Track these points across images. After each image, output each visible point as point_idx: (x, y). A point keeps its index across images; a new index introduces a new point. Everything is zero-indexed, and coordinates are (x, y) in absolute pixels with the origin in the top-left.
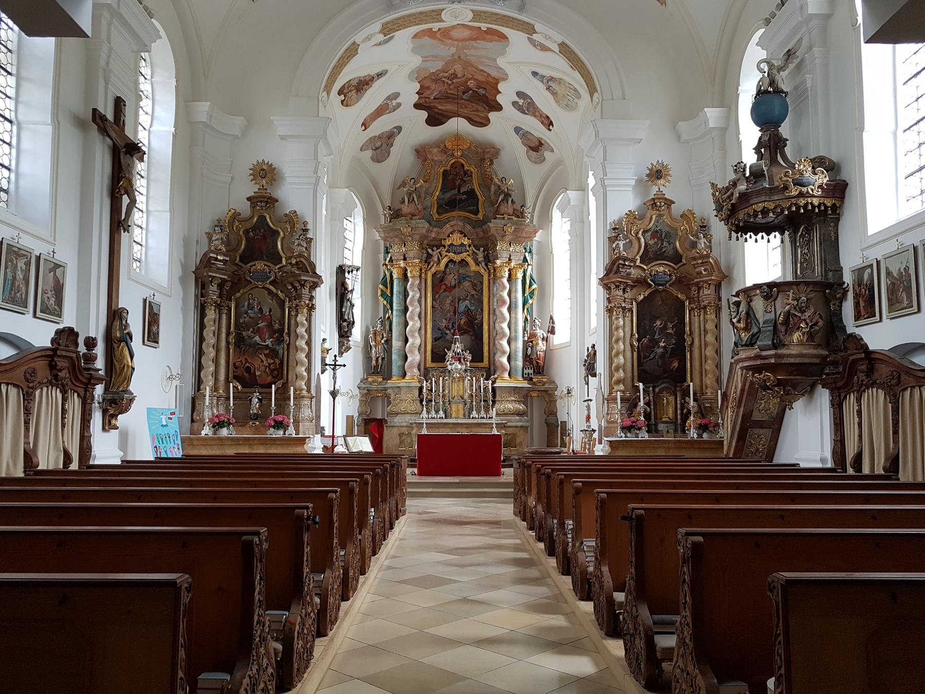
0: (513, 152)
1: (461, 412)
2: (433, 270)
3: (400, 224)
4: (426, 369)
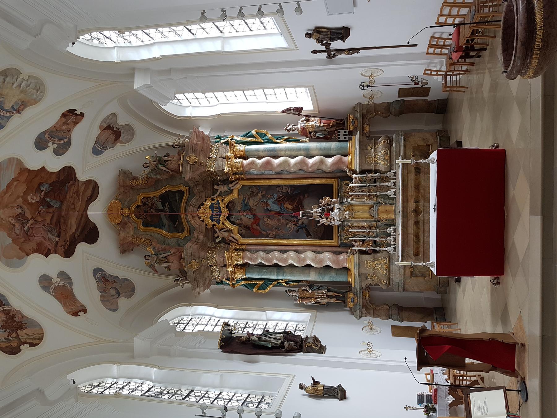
0: (119, 157)
1: (388, 208)
2: (237, 237)
3: (192, 267)
4: (339, 246)
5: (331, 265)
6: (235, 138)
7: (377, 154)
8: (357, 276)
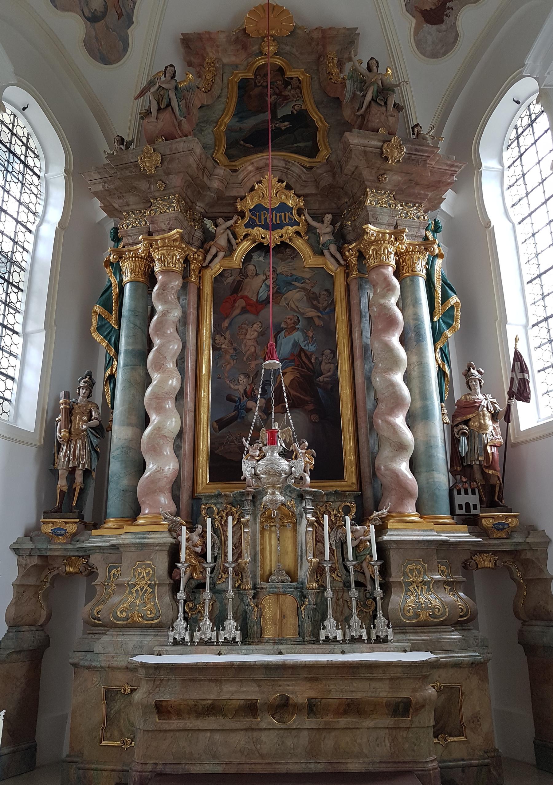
1: (291, 622)
2: (216, 268)
4: (195, 499)
5: (146, 474)
6: (439, 262)
7: (429, 589)
8: (114, 541)
